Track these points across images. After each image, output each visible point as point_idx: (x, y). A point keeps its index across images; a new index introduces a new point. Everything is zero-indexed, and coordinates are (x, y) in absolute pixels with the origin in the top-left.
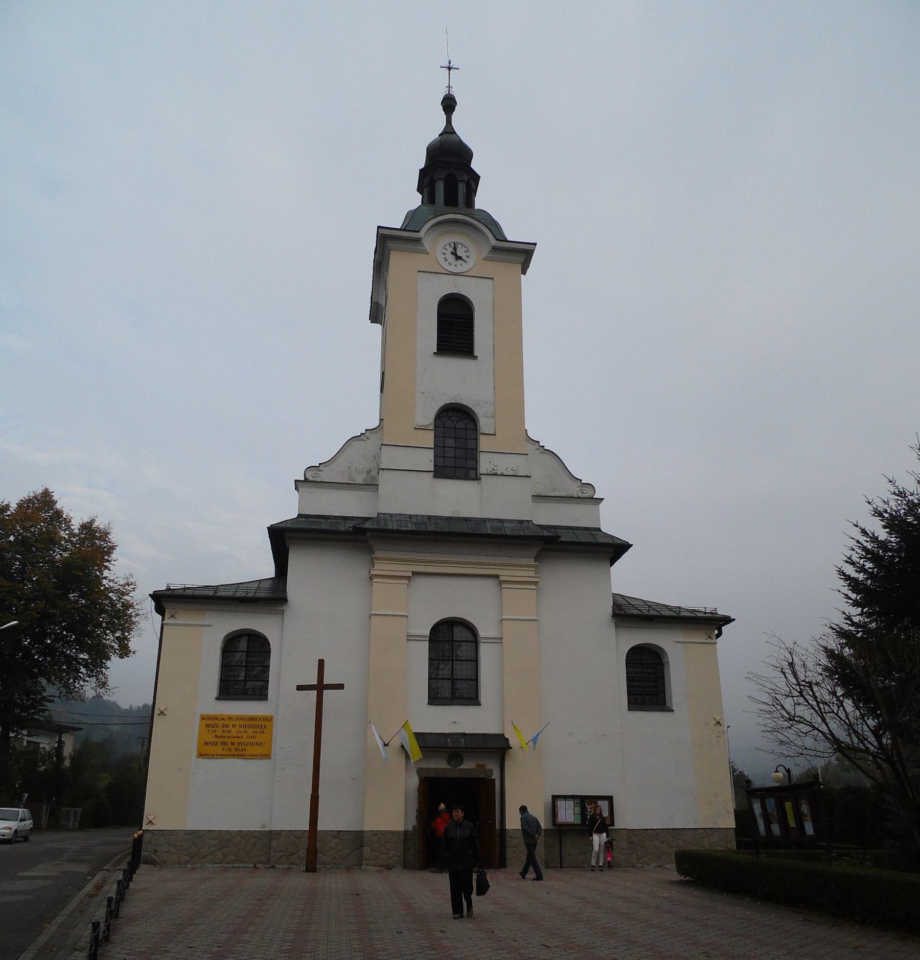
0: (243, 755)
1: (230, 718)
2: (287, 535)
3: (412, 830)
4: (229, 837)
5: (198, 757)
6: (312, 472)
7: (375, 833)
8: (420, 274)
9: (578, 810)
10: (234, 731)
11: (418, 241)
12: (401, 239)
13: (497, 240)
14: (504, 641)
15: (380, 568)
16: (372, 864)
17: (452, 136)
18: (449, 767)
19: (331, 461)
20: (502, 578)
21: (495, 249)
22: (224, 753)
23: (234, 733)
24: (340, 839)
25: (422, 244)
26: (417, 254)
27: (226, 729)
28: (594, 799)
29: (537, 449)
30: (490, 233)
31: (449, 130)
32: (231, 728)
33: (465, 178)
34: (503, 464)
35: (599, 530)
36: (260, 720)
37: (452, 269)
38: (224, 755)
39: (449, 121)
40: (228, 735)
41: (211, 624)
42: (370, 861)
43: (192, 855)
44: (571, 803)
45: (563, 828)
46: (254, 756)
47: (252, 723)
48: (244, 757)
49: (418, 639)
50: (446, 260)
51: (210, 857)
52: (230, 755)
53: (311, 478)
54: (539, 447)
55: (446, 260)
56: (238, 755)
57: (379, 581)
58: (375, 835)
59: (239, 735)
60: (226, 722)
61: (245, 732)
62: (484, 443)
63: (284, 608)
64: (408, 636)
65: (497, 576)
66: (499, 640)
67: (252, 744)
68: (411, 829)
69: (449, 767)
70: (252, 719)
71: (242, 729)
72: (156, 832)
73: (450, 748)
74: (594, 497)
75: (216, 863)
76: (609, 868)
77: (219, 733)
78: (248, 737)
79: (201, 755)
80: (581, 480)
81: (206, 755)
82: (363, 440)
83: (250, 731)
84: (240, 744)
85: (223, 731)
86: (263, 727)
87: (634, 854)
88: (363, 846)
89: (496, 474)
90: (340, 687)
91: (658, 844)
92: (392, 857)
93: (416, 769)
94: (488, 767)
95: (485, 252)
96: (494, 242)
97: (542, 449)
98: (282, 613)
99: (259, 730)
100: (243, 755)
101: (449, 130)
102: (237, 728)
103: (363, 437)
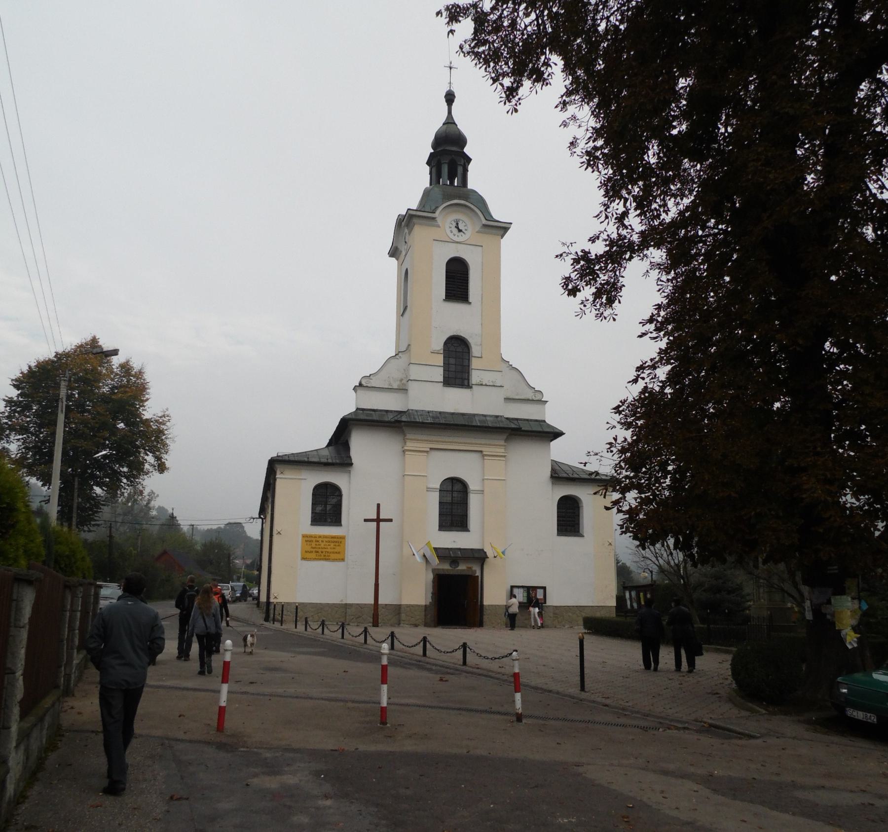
1: (320, 537)
7: (408, 606)
8: (435, 241)
15: (410, 445)
20: (484, 453)
21: (485, 226)
23: (322, 545)
27: (317, 543)
31: (450, 121)
34: (487, 378)
37: (456, 239)
44: (521, 590)
47: (333, 540)
50: (452, 232)
55: (452, 232)
56: (325, 559)
60: (318, 539)
61: (329, 545)
62: (475, 363)
65: (481, 452)
66: (482, 492)
67: (333, 553)
70: (333, 537)
71: (327, 544)
77: (314, 546)
78: (331, 548)
79: (303, 559)
80: (534, 388)
83: (332, 544)
89: (482, 385)
94: (474, 569)
95: (478, 228)
96: (484, 222)
99: (337, 544)
101: (450, 121)
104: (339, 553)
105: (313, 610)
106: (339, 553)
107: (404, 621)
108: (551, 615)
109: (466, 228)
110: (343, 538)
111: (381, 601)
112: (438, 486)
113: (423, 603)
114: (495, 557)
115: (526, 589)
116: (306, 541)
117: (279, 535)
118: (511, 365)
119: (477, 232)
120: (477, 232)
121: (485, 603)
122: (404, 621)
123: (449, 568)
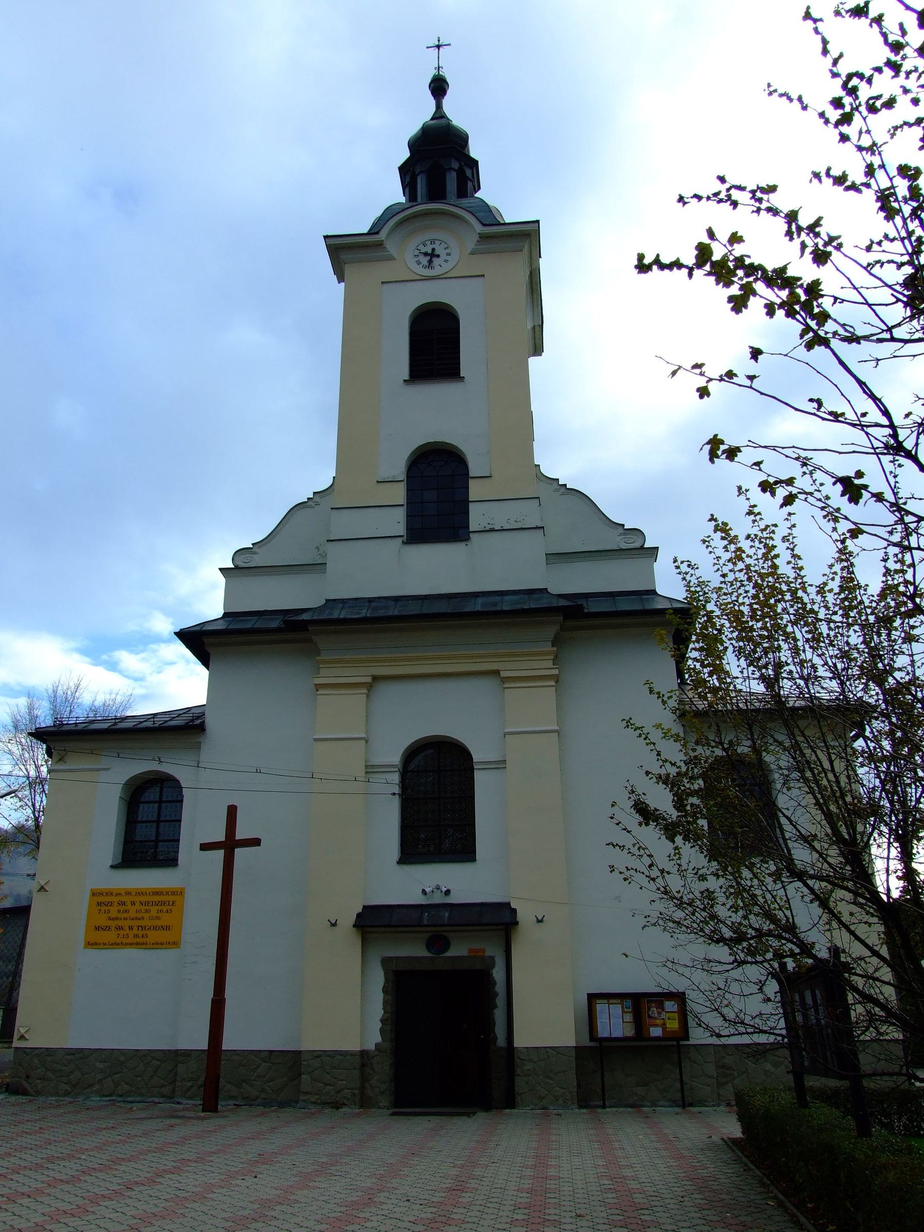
0: (143, 944)
1: (128, 893)
2: (207, 640)
3: (373, 1048)
4: (122, 1059)
5: (85, 947)
6: (243, 556)
7: (318, 1055)
8: (385, 286)
9: (629, 1017)
10: (132, 909)
11: (379, 245)
12: (368, 246)
13: (484, 225)
14: (508, 765)
15: (327, 675)
16: (313, 1100)
17: (443, 121)
18: (430, 955)
19: (268, 539)
20: (503, 674)
21: (483, 238)
22: (119, 941)
23: (132, 914)
24: (272, 1063)
25: (386, 248)
26: (381, 262)
27: (122, 908)
28: (659, 998)
29: (556, 490)
30: (473, 218)
31: (439, 114)
32: (129, 907)
33: (455, 165)
34: (499, 515)
35: (653, 592)
36: (167, 893)
38: (119, 944)
39: (439, 106)
40: (125, 915)
41: (108, 767)
42: (309, 1096)
43: (74, 1083)
44: (617, 1009)
45: (604, 1044)
46: (157, 943)
47: (156, 898)
48: (144, 946)
49: (388, 770)
51: (97, 1087)
52: (126, 944)
53: (241, 565)
54: (559, 487)
56: (138, 944)
57: (334, 692)
58: (317, 1057)
59: (139, 915)
60: (122, 899)
61: (147, 911)
62: (475, 490)
63: (201, 740)
64: (366, 767)
65: (496, 673)
66: (500, 765)
67: (155, 928)
68: (372, 1047)
69: (430, 955)
70: (157, 893)
71: (143, 908)
72: (29, 1050)
73: (425, 926)
74: (646, 546)
75: (104, 1096)
76: (684, 1106)
77: (114, 914)
78: (151, 918)
79: (90, 944)
80: (623, 525)
81: (96, 944)
82: (312, 507)
83: (154, 909)
84: (140, 928)
85: (119, 911)
86: (171, 903)
87: (730, 1084)
88: (300, 1075)
89: (492, 530)
90: (256, 842)
91: (768, 1067)
92: (342, 1090)
93: (380, 958)
94: (488, 953)
96: (479, 228)
97: (563, 490)
98: (198, 747)
99: (165, 908)
100: (143, 944)
101: (439, 114)
102: (137, 907)
103: (311, 503)
104: (167, 928)
105: (101, 1066)
106: (167, 928)
107: (306, 1093)
108: (711, 1070)
109: (448, 251)
110: (179, 893)
111: (229, 1043)
112: (396, 758)
113: (571, 1042)
114: (539, 921)
115: (629, 1003)
116: (99, 904)
117: (43, 893)
118: (565, 485)
119: (472, 253)
120: (472, 253)
121: (518, 1043)
122: (306, 1093)
123: (426, 954)
